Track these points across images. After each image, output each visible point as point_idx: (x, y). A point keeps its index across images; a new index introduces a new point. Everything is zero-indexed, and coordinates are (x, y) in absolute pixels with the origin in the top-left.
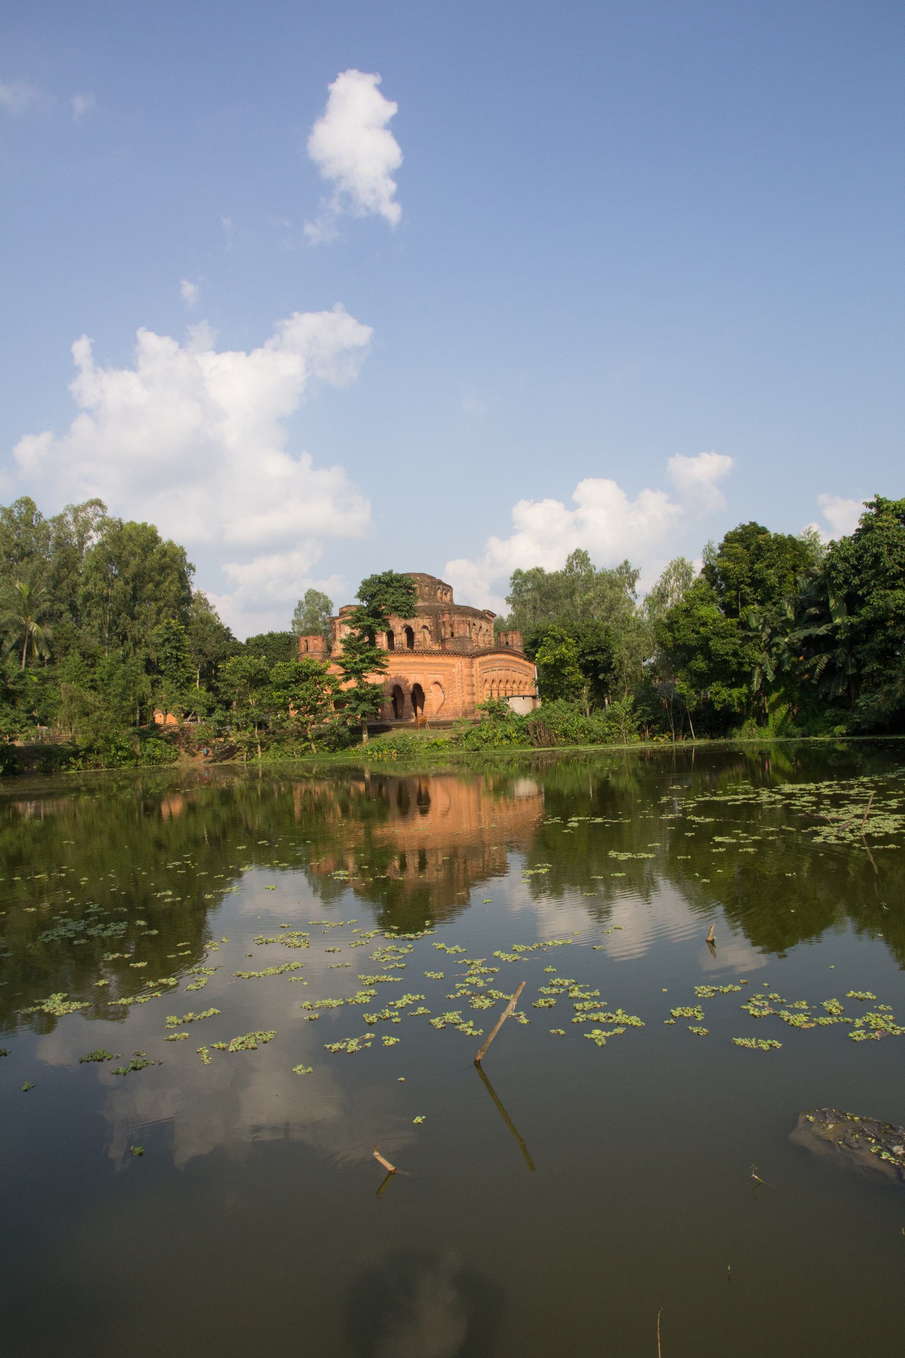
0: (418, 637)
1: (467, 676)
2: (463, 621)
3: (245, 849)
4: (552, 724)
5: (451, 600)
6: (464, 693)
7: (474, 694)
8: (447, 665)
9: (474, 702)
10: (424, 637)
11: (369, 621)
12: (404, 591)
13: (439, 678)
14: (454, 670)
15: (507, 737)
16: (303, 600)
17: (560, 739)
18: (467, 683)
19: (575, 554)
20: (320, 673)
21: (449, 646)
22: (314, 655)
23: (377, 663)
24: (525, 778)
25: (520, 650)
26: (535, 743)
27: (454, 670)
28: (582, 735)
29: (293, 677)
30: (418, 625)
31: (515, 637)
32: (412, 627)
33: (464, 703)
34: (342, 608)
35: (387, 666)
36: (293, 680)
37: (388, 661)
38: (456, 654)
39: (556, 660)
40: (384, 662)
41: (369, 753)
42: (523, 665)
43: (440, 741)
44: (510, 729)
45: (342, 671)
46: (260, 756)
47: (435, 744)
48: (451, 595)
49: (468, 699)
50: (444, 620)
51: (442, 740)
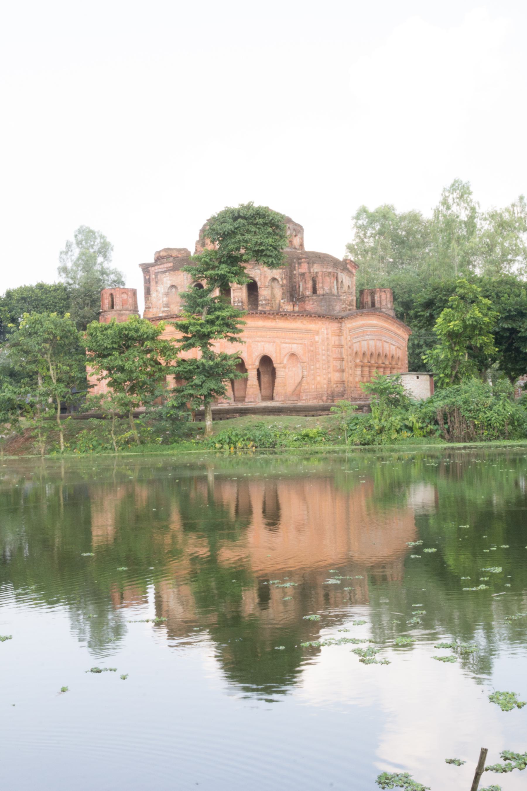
0: (264, 293)
1: (334, 346)
2: (330, 273)
3: (507, 549)
4: (470, 411)
5: (302, 245)
6: (331, 370)
7: (343, 371)
8: (308, 331)
9: (343, 382)
10: (272, 294)
11: (224, 269)
12: (270, 230)
13: (296, 348)
14: (317, 338)
15: (411, 429)
16: (73, 240)
17: (481, 432)
18: (335, 356)
19: (453, 185)
20: (153, 337)
21: (310, 306)
22: (122, 315)
23: (228, 325)
24: (426, 484)
25: (392, 313)
26: (447, 436)
27: (317, 338)
28: (510, 427)
29: (115, 343)
30: (265, 277)
31: (383, 297)
32: (257, 279)
33: (329, 381)
34: (160, 252)
35: (241, 331)
36: (115, 346)
37: (245, 323)
38: (321, 316)
39: (465, 327)
40: (238, 326)
41: (218, 446)
42: (396, 333)
43: (312, 432)
44: (412, 418)
45: (180, 335)
46: (63, 448)
47: (307, 435)
48: (302, 239)
49: (336, 376)
50: (302, 271)
51: (315, 430)
